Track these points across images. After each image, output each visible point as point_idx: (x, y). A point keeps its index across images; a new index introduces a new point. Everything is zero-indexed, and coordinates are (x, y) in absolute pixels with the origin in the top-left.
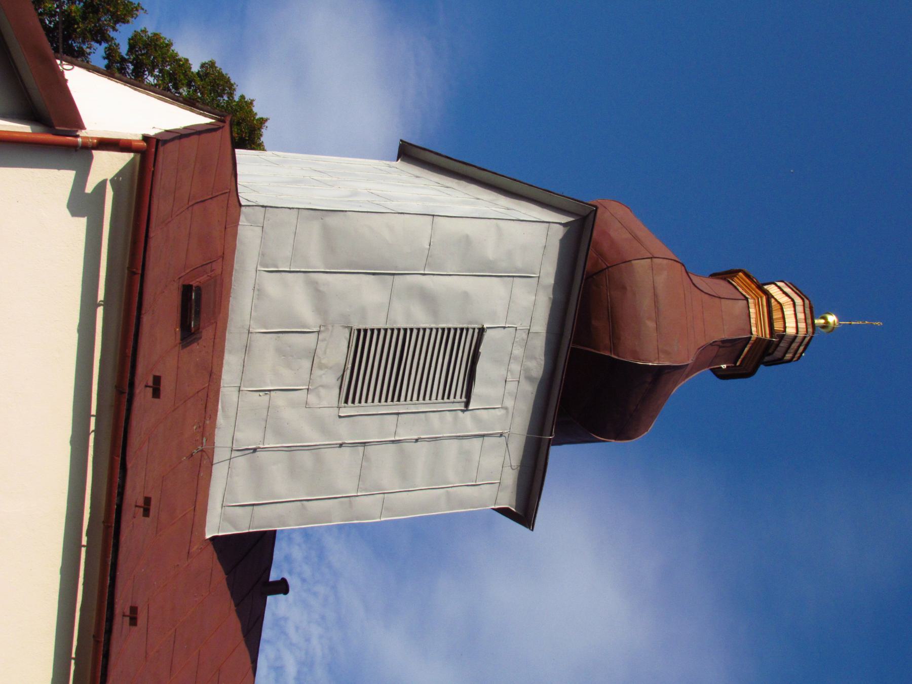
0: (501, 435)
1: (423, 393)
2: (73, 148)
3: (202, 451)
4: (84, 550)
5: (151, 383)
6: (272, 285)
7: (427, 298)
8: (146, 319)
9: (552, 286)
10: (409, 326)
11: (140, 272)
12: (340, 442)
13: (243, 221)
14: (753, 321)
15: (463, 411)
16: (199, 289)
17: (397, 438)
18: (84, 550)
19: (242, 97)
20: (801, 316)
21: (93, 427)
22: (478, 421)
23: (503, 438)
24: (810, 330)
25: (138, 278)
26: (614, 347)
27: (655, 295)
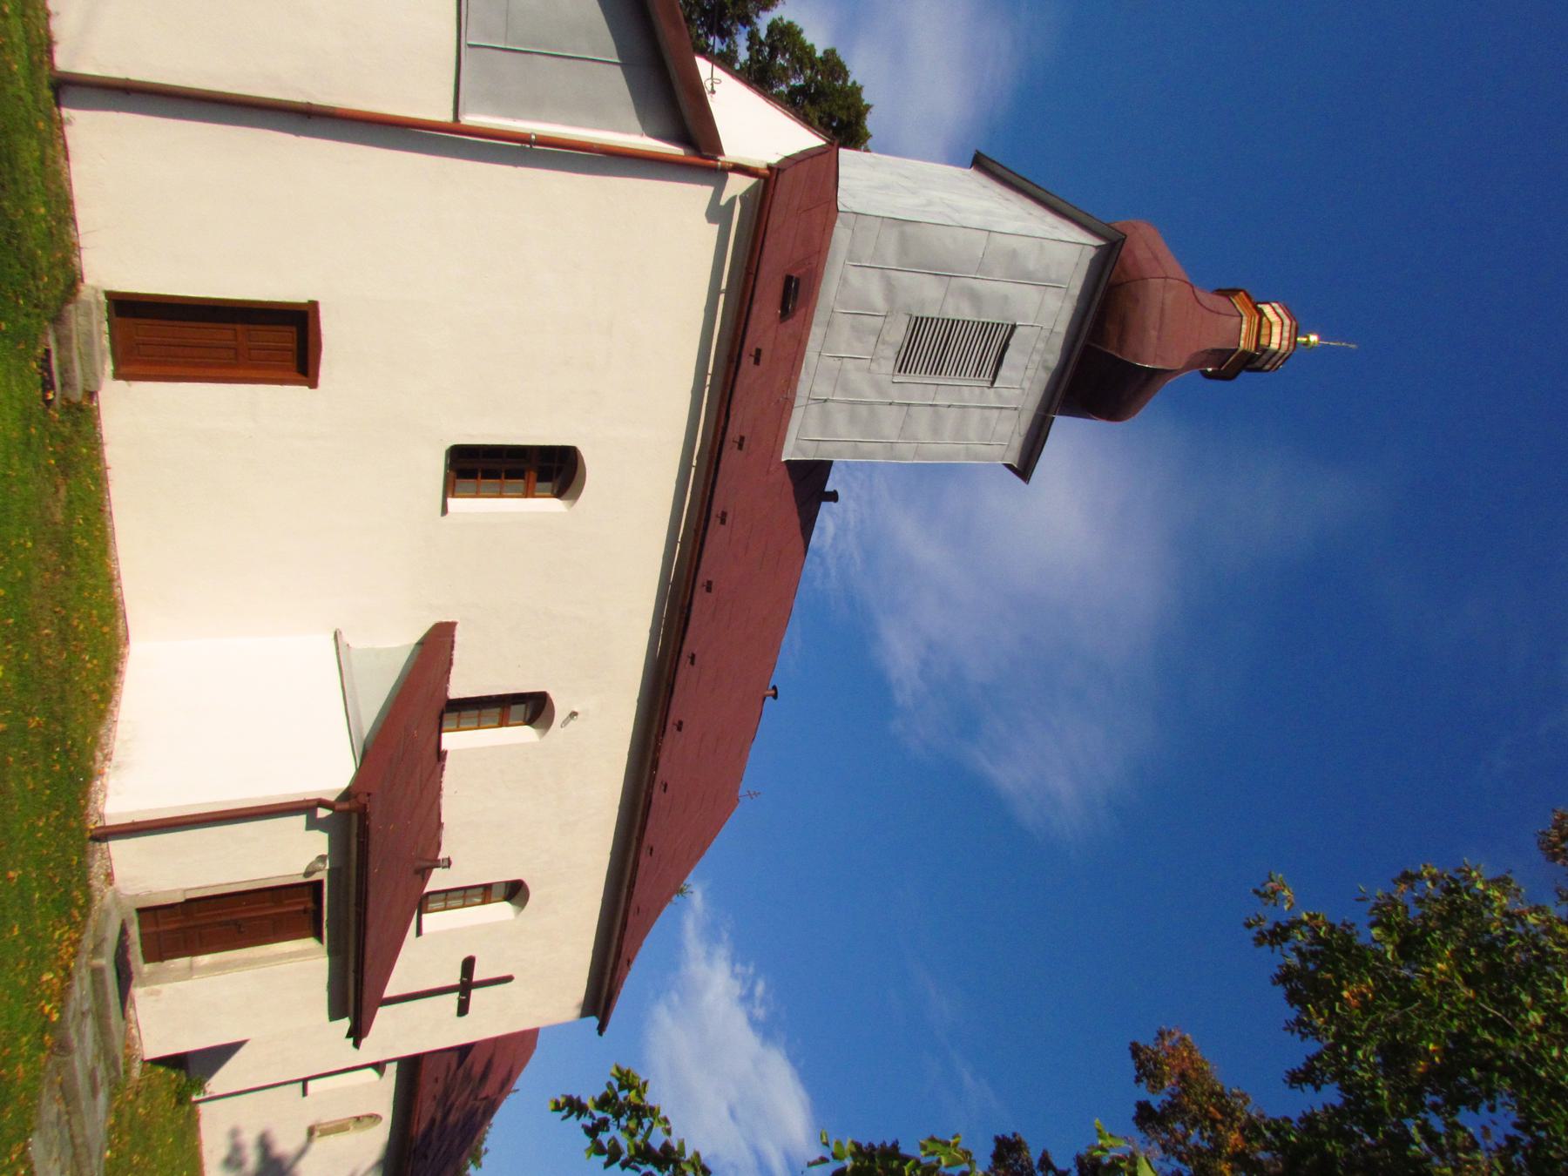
0: (1016, 409)
1: (959, 371)
2: (714, 169)
3: (787, 398)
4: (693, 470)
5: (754, 353)
6: (855, 277)
7: (975, 298)
8: (755, 308)
9: (1076, 297)
10: (957, 317)
11: (754, 272)
12: (890, 401)
13: (838, 224)
14: (1243, 335)
15: (989, 388)
16: (798, 281)
17: (934, 403)
18: (693, 470)
19: (854, 83)
20: (1286, 335)
21: (708, 382)
22: (999, 396)
23: (1017, 412)
24: (1291, 347)
25: (752, 277)
26: (1120, 350)
27: (1162, 310)
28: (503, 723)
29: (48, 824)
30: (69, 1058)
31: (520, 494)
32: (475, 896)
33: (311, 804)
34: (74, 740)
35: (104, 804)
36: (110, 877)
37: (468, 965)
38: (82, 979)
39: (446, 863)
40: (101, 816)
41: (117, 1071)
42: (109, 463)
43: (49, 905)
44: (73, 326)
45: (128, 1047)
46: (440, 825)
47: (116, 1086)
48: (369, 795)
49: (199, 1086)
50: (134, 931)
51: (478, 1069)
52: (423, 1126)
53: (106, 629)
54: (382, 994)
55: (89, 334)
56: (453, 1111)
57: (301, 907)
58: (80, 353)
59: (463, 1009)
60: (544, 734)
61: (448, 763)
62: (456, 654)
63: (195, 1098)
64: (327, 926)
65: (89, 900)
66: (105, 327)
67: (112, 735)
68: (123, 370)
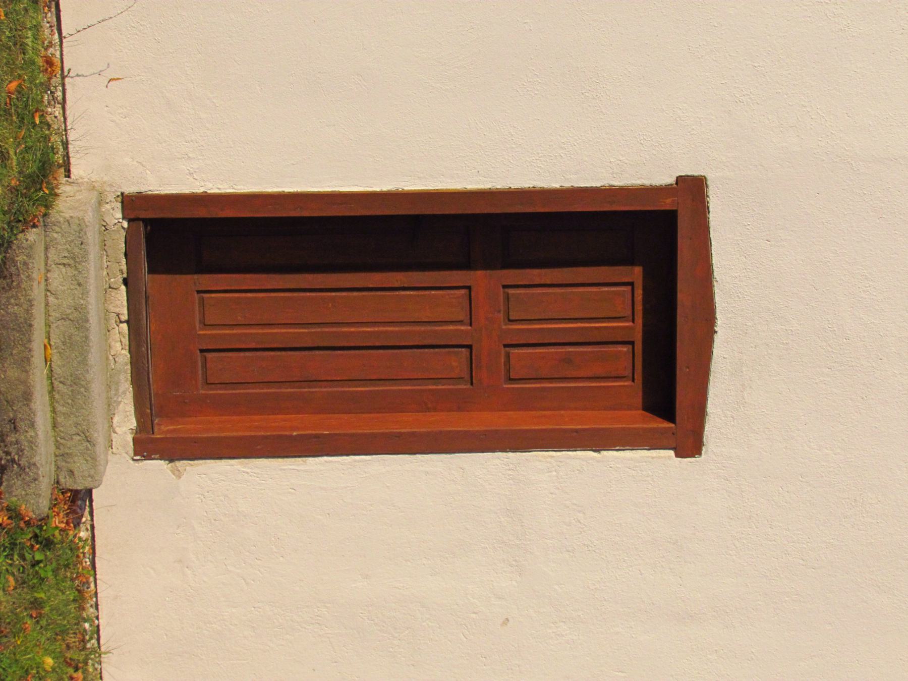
44: (37, 292)
55: (80, 321)
58: (51, 375)
66: (120, 300)
68: (163, 429)
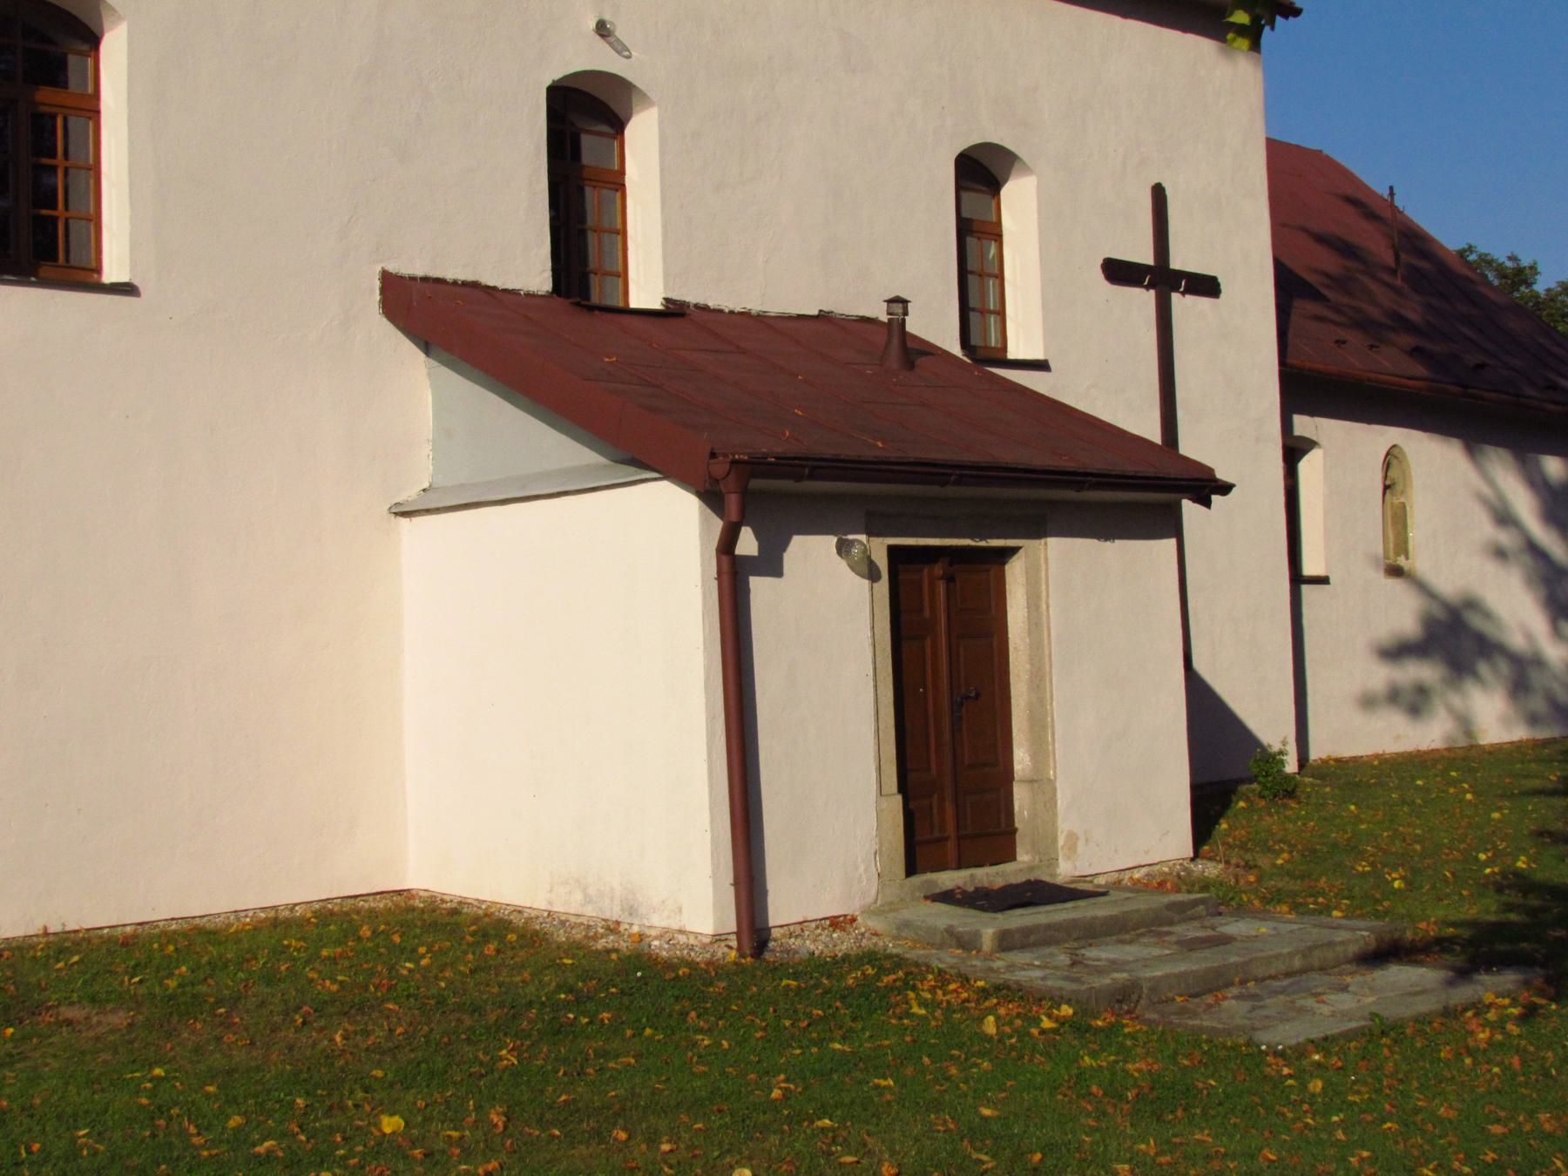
28: (616, 182)
29: (708, 1032)
30: (1146, 987)
31: (91, 124)
32: (983, 254)
33: (725, 567)
34: (559, 988)
35: (696, 935)
36: (835, 923)
37: (1119, 272)
38: (1011, 967)
39: (898, 308)
40: (718, 938)
41: (1195, 903)
42: (34, 929)
43: (860, 1025)
45: (1161, 884)
46: (824, 317)
47: (1223, 901)
48: (713, 455)
49: (1272, 760)
50: (949, 879)
51: (1330, 262)
52: (1419, 370)
53: (366, 931)
54: (1157, 445)
56: (1403, 312)
57: (941, 587)
59: (1206, 286)
60: (644, 97)
61: (692, 296)
62: (454, 272)
63: (1291, 766)
64: (983, 538)
65: (871, 957)
67: (573, 919)
